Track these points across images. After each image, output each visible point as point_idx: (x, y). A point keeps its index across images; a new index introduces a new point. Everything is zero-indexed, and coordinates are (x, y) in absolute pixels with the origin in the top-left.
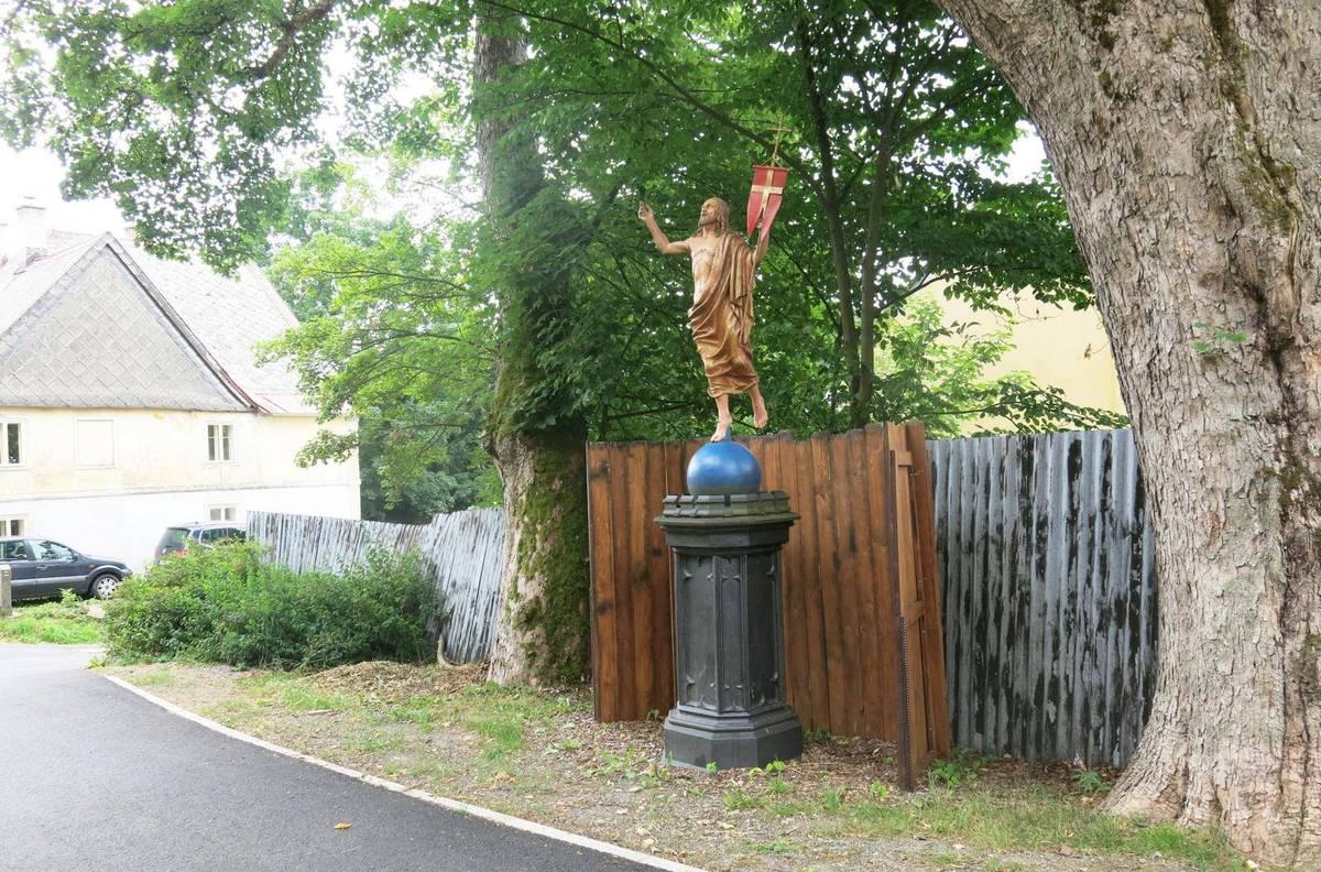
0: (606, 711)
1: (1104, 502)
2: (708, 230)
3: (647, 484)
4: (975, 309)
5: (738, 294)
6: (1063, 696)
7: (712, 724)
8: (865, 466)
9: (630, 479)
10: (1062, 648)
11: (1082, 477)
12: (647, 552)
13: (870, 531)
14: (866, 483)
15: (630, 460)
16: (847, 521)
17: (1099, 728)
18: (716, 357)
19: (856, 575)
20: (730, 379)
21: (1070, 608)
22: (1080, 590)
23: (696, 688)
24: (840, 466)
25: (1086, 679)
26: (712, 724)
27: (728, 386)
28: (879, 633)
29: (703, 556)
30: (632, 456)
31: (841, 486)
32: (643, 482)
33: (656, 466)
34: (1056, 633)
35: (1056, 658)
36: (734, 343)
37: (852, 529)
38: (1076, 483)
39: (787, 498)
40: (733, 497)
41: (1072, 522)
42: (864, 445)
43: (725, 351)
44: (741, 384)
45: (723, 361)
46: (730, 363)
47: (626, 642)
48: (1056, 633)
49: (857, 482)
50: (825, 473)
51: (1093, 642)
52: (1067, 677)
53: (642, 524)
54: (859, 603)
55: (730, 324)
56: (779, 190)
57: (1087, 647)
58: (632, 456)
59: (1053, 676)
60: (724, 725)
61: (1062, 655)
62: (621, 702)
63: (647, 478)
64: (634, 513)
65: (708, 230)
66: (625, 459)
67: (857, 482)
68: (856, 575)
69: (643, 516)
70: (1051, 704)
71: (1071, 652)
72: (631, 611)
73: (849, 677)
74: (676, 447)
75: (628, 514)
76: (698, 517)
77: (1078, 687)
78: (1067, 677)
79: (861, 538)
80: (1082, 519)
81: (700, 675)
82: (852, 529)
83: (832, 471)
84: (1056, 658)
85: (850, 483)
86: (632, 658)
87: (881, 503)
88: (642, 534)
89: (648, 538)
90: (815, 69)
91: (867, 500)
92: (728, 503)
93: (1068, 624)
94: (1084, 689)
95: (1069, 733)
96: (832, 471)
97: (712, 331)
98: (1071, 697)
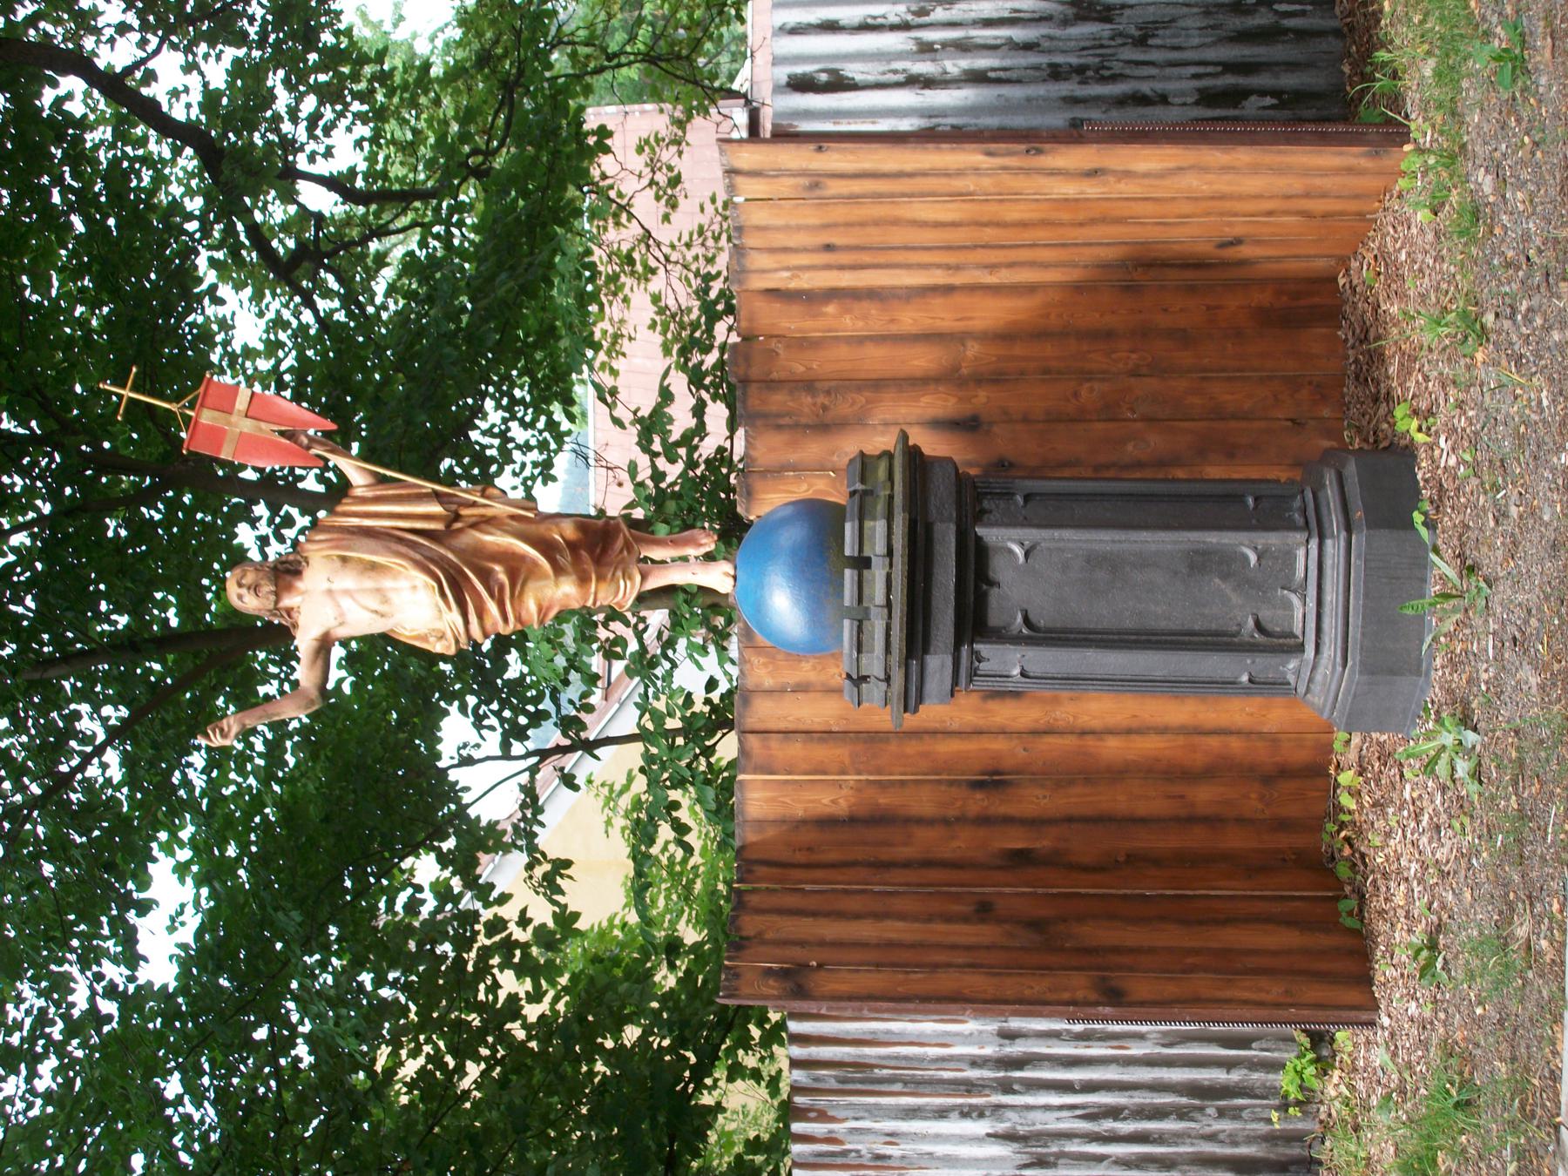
0: (1352, 996)
1: (894, 28)
4: (554, 479)
5: (436, 509)
6: (1230, 80)
7: (1335, 549)
10: (1145, 88)
11: (853, 71)
12: (983, 921)
15: (769, 935)
17: (1276, 12)
19: (1026, 420)
21: (1076, 78)
22: (1043, 60)
23: (1266, 614)
25: (1196, 41)
26: (1335, 549)
28: (1135, 373)
29: (976, 565)
30: (760, 934)
34: (1121, 102)
35: (1163, 99)
38: (859, 78)
39: (862, 454)
41: (927, 83)
42: (771, 384)
44: (620, 543)
47: (1189, 960)
48: (1121, 102)
51: (1133, 31)
52: (1196, 76)
53: (916, 925)
54: (1080, 418)
57: (1141, 42)
59: (1197, 103)
60: (1334, 521)
61: (1159, 86)
62: (1271, 197)
63: (814, 914)
64: (894, 936)
66: (764, 942)
68: (1026, 420)
70: (1246, 103)
71: (1153, 71)
72: (1116, 950)
73: (1231, 452)
74: (750, 871)
75: (891, 945)
76: (889, 605)
77: (1211, 54)
78: (1196, 76)
80: (924, 67)
81: (1235, 599)
84: (1163, 99)
86: (1225, 952)
88: (941, 927)
89: (949, 919)
90: (49, 1143)
93: (1103, 80)
94: (1214, 44)
95: (1292, 66)
98: (1229, 67)
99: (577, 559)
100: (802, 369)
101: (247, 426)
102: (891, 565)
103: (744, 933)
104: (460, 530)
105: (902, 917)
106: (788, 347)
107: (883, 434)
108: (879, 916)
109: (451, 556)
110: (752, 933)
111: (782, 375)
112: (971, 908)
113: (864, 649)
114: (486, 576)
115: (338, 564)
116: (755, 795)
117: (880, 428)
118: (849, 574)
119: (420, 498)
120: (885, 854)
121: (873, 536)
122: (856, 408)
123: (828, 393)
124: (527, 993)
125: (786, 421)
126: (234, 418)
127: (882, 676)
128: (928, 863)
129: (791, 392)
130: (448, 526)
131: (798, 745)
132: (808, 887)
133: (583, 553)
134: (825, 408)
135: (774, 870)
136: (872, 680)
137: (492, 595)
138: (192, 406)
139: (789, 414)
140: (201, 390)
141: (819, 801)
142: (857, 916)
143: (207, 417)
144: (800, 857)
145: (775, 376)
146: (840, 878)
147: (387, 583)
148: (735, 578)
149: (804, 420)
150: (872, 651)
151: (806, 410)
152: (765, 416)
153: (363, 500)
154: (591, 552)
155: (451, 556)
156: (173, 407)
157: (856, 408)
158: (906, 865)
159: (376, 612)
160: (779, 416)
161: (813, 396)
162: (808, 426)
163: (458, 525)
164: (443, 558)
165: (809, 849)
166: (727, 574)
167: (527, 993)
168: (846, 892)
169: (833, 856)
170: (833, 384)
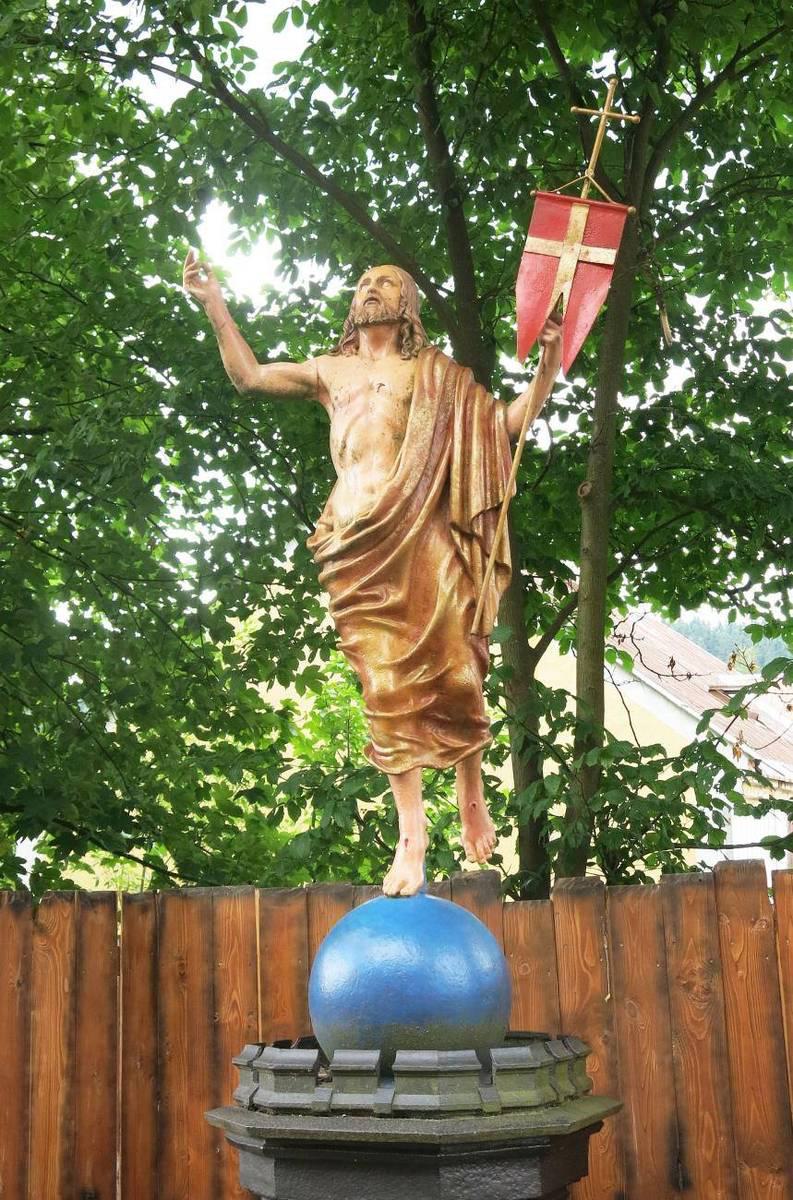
2: (377, 342)
3: (75, 1009)
5: (476, 504)
8: (717, 965)
9: (35, 993)
13: (732, 1135)
14: (720, 1013)
15: (39, 942)
16: (660, 1110)
18: (404, 668)
20: (429, 729)
24: (642, 969)
27: (425, 747)
30: (42, 930)
31: (643, 1019)
32: (65, 1005)
33: (97, 962)
36: (456, 629)
37: (677, 1137)
40: (497, 1053)
43: (432, 651)
44: (455, 742)
45: (419, 676)
46: (438, 684)
49: (692, 1008)
50: (595, 983)
55: (444, 579)
56: (608, 256)
58: (42, 930)
63: (76, 993)
64: (41, 1092)
65: (377, 342)
66: (26, 936)
67: (692, 1008)
69: (61, 1099)
74: (144, 909)
79: (702, 1153)
82: (677, 1137)
83: (618, 983)
85: (670, 1010)
87: (764, 1058)
88: (56, 1151)
89: (70, 1160)
91: (722, 1055)
92: (485, 1070)
96: (618, 983)
97: (395, 596)
99: (421, 690)
100: (736, 956)
101: (567, 265)
102: (382, 1116)
103: (42, 912)
104: (452, 542)
105: (72, 1100)
106: (763, 937)
107: (661, 1063)
108: (73, 1074)
109: (412, 533)
110: (41, 920)
111: (727, 932)
112: (89, 1186)
113: (281, 1079)
114: (391, 576)
115: (402, 395)
116: (239, 909)
117: (667, 1060)
118: (372, 1057)
119: (493, 488)
120: (176, 1071)
121: (420, 1091)
122: (691, 1027)
123: (708, 991)
124: (232, 648)
125: (670, 937)
126: (578, 247)
127: (256, 1100)
128: (162, 1124)
129: (705, 942)
130: (454, 526)
131: (294, 962)
132: (120, 979)
133: (433, 698)
134: (689, 987)
135: (147, 938)
136: (256, 1085)
137: (363, 588)
138: (594, 195)
139: (678, 941)
140: (614, 204)
141: (234, 988)
142: (72, 1045)
143: (579, 215)
144: (169, 966)
145: (726, 920)
146: (136, 1018)
147: (377, 457)
148: (397, 895)
149: (672, 961)
150: (278, 1089)
151: (685, 962)
152: (674, 911)
153: (487, 419)
154: (435, 707)
155: (412, 533)
156: (590, 173)
157: (691, 1027)
158: (159, 1095)
159: (344, 447)
160: (676, 927)
161: (702, 972)
162: (665, 965)
163: (457, 538)
164: (410, 523)
165: (183, 976)
166: (403, 884)
167: (232, 648)
168: (113, 1027)
169: (171, 1004)
170: (720, 996)
